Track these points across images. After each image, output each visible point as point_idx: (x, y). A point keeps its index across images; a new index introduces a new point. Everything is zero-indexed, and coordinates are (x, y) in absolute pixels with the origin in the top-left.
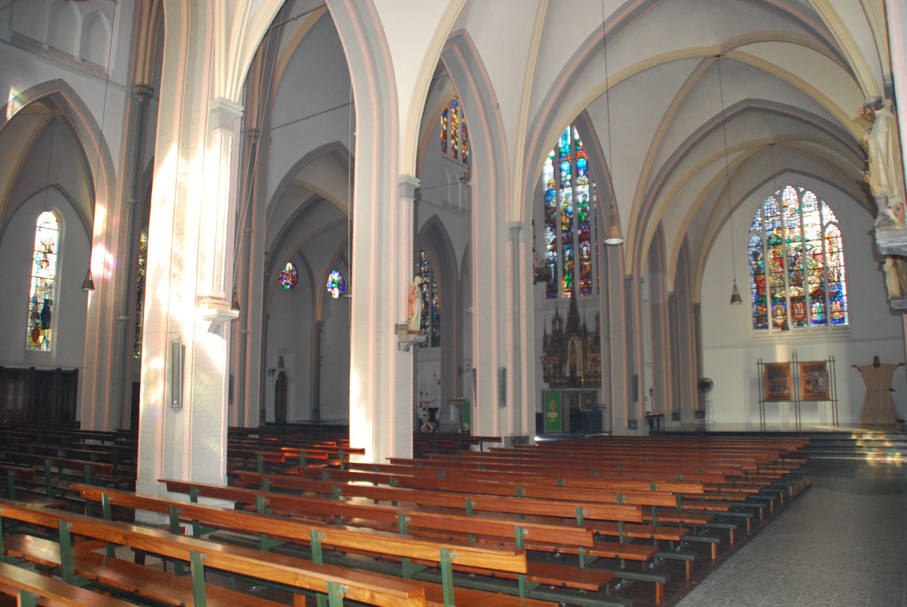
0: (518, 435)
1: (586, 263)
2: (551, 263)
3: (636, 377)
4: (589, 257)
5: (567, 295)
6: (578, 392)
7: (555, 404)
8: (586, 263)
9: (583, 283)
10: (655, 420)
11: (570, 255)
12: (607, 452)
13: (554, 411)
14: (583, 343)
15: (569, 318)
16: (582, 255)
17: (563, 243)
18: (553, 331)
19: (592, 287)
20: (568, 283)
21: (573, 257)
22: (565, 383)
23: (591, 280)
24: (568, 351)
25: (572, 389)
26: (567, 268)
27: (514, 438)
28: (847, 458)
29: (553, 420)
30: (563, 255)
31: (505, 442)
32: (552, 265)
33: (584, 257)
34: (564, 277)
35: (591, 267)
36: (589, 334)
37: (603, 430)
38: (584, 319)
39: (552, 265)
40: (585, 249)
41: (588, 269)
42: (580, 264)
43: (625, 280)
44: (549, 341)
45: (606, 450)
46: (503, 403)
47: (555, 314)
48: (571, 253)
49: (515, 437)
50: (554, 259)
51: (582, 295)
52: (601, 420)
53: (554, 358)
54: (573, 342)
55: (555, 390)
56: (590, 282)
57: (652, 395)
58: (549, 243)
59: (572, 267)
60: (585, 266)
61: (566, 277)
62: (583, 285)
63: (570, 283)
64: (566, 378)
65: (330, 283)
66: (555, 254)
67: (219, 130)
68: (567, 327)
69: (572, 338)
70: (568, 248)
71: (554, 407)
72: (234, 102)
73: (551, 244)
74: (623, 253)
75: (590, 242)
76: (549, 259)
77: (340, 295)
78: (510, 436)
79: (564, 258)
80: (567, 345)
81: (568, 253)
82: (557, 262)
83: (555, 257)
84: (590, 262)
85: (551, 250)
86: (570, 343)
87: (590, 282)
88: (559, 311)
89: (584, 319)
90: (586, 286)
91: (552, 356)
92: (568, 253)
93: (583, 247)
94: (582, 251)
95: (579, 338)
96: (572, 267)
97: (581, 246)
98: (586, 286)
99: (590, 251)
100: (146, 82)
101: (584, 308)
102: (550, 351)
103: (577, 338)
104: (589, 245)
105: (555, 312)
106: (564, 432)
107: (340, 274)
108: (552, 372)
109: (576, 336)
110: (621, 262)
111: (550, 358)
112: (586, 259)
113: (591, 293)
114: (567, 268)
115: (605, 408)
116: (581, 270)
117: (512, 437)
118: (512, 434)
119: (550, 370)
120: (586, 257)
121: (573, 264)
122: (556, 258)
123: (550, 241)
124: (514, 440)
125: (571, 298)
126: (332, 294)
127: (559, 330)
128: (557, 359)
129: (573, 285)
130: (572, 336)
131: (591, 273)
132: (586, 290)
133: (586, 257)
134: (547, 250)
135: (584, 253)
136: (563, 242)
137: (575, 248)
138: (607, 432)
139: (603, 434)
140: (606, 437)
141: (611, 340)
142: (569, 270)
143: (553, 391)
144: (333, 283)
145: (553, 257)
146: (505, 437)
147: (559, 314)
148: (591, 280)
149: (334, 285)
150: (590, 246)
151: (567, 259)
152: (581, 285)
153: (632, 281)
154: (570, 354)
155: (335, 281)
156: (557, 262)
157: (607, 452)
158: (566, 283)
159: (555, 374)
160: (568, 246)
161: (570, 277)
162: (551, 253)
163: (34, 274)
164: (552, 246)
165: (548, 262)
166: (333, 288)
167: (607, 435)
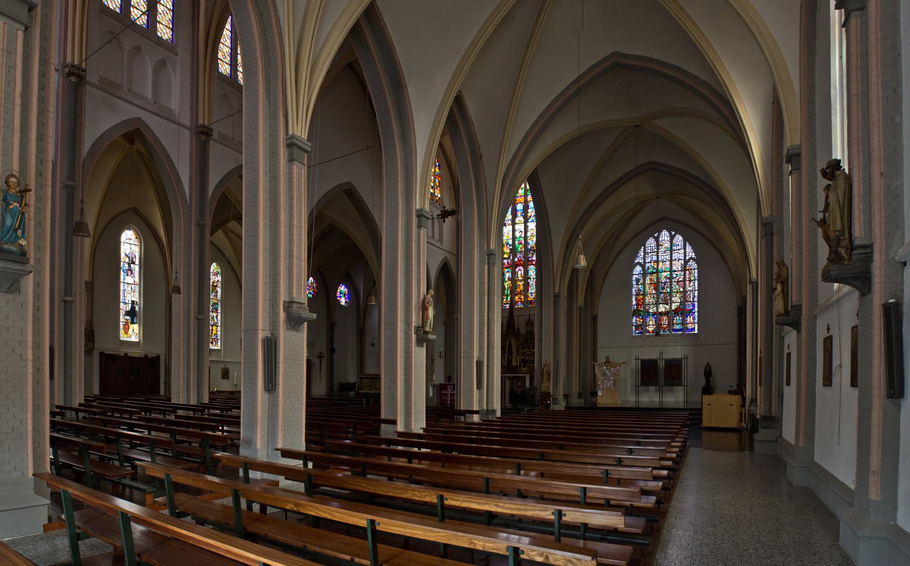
1: (520, 283)
8: (520, 283)
15: (507, 324)
43: (554, 296)
54: (510, 341)
69: (510, 338)
90: (519, 300)
98: (519, 300)
100: (206, 124)
109: (513, 336)
115: (537, 389)
144: (341, 293)
158: (506, 298)
163: (122, 280)
166: (340, 297)
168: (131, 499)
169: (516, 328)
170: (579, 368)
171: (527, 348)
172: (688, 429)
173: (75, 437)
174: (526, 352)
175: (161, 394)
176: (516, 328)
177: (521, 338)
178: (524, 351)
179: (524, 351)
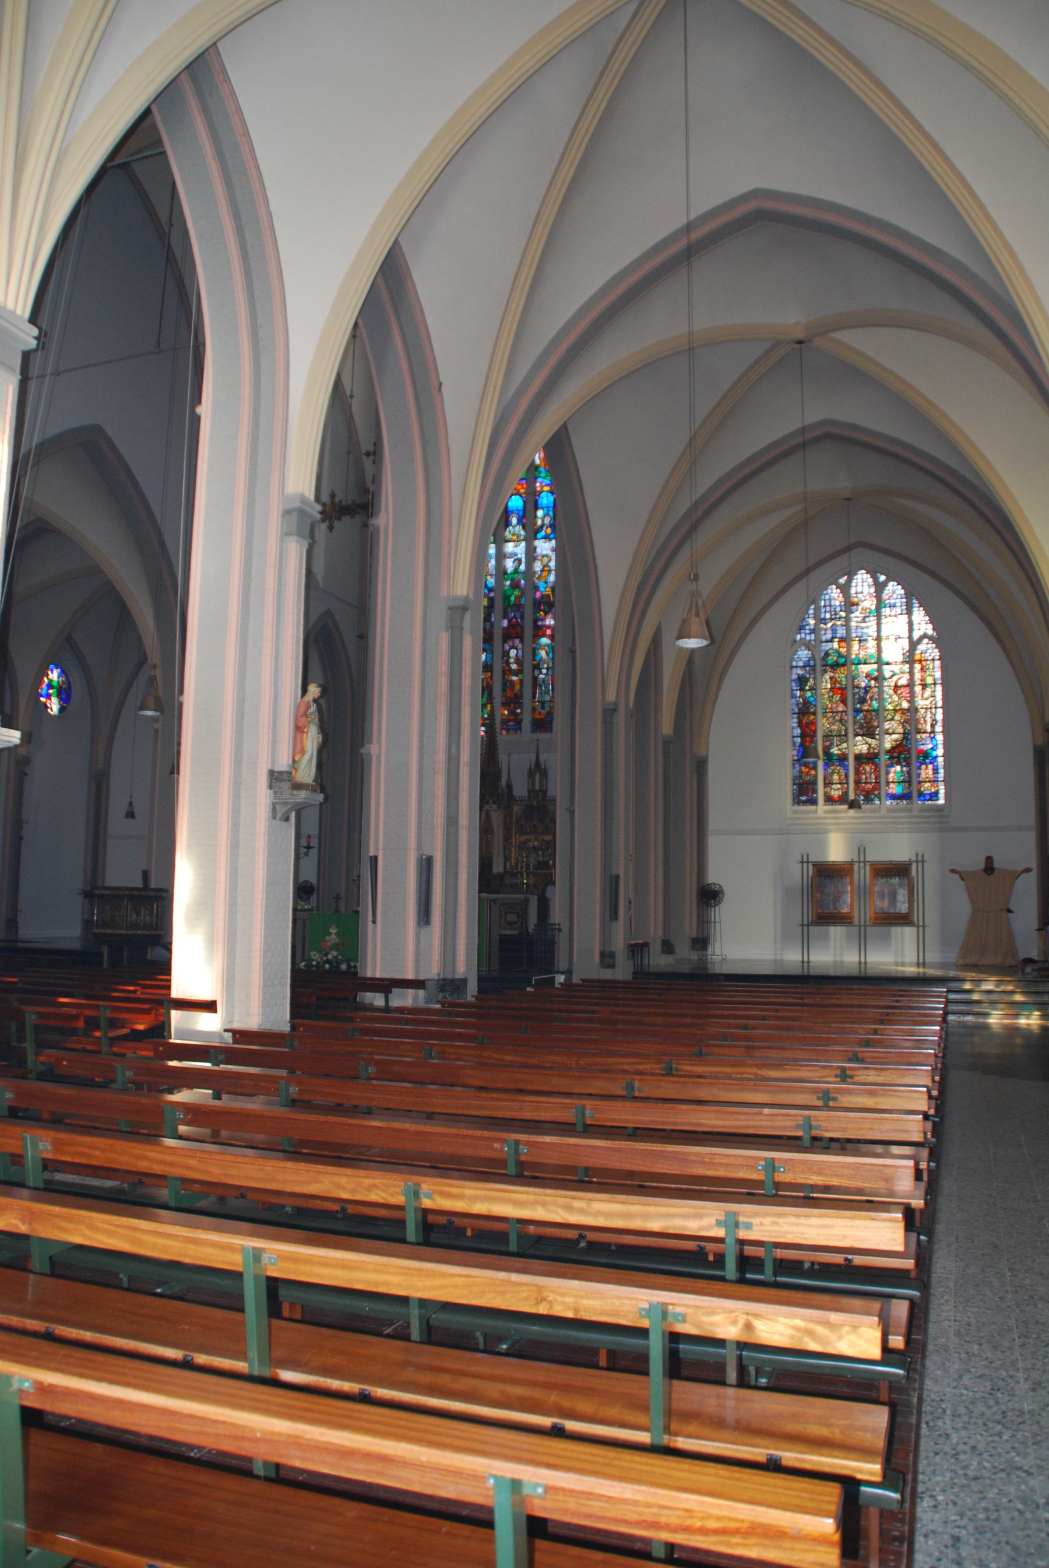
0: (449, 976)
3: (617, 877)
8: (514, 678)
9: (506, 712)
11: (486, 661)
14: (505, 817)
16: (508, 663)
19: (521, 721)
21: (491, 666)
37: (556, 969)
41: (518, 687)
43: (604, 711)
46: (425, 919)
49: (443, 980)
51: (504, 732)
56: (519, 711)
59: (488, 683)
60: (512, 682)
65: (44, 687)
67: (295, 538)
72: (22, 318)
74: (603, 663)
75: (522, 641)
77: (62, 710)
78: (436, 977)
84: (520, 676)
87: (519, 711)
90: (511, 717)
94: (509, 657)
95: (499, 808)
96: (488, 683)
97: (507, 647)
98: (511, 717)
99: (523, 656)
103: (495, 807)
104: (520, 646)
107: (63, 672)
109: (494, 802)
112: (514, 670)
113: (520, 729)
115: (560, 930)
116: (504, 690)
117: (438, 980)
118: (439, 974)
120: (514, 667)
121: (491, 677)
124: (443, 986)
126: (47, 707)
131: (522, 695)
132: (512, 723)
135: (512, 660)
144: (50, 686)
149: (51, 691)
150: (523, 648)
155: (55, 684)
166: (48, 696)
169: (504, 783)
176: (504, 783)
177: (516, 808)
178: (523, 838)
179: (523, 838)
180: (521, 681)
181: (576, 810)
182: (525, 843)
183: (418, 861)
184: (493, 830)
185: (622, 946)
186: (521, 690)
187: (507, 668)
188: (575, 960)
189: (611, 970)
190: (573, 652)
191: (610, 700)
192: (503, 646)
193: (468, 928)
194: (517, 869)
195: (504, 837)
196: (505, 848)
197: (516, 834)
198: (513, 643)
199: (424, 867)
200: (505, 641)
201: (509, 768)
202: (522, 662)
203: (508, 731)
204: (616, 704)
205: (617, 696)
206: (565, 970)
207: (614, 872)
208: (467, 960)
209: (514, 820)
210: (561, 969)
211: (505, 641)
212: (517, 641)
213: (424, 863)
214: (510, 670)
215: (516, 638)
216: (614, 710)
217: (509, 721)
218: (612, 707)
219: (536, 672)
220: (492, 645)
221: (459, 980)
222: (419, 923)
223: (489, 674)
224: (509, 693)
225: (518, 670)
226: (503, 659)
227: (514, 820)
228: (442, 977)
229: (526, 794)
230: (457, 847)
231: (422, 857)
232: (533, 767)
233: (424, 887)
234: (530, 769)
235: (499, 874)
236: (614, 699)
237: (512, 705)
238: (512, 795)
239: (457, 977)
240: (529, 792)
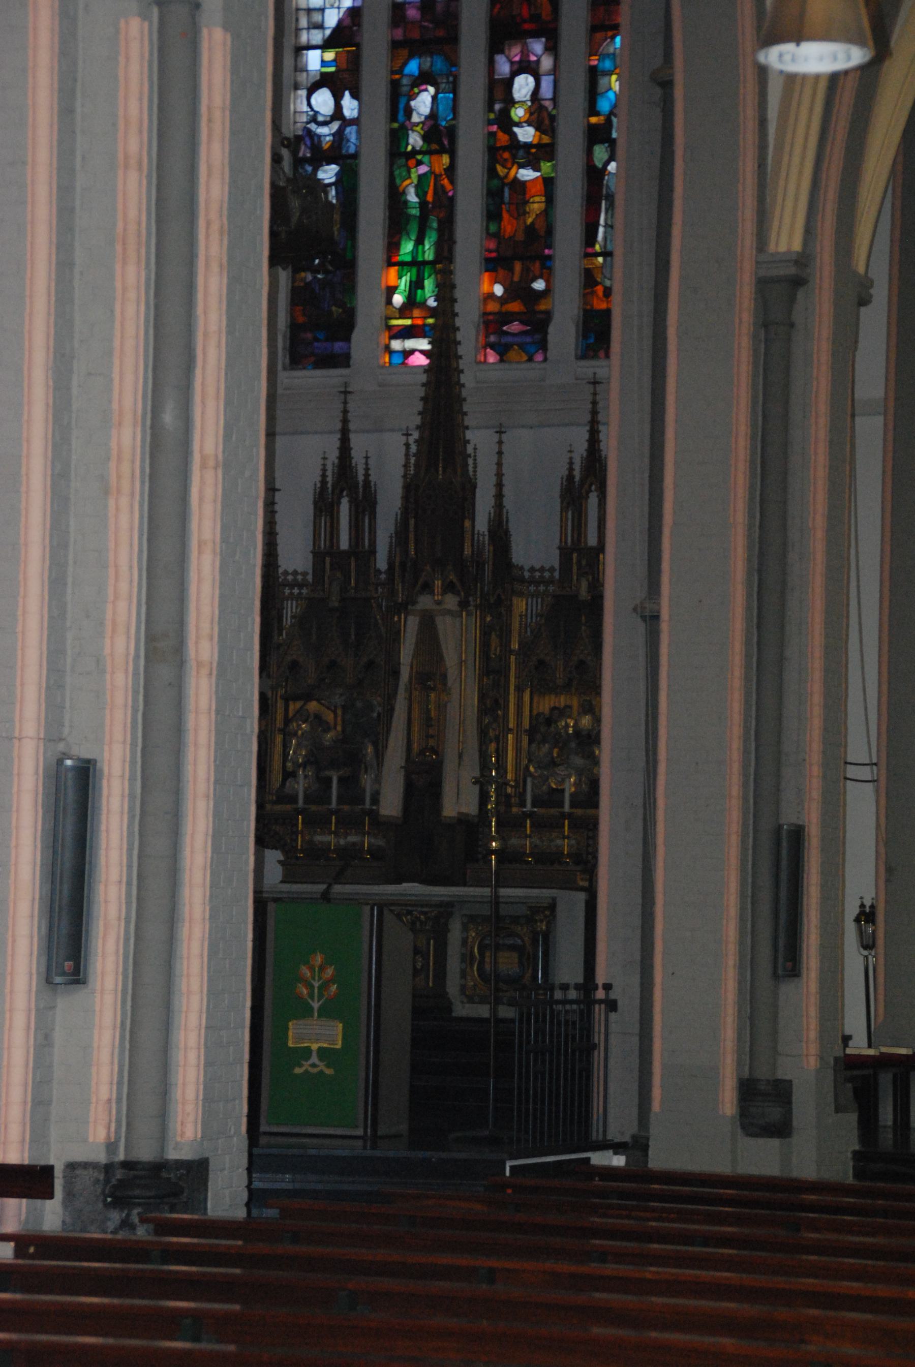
0: (145, 1153)
1: (527, 174)
2: (321, 157)
3: (798, 834)
4: (546, 140)
5: (408, 353)
6: (446, 909)
7: (330, 972)
8: (527, 174)
9: (498, 290)
10: (886, 1080)
11: (433, 116)
12: (611, 1269)
13: (325, 1012)
14: (486, 633)
15: (409, 488)
16: (506, 123)
17: (395, 45)
18: (318, 556)
19: (547, 317)
20: (416, 285)
21: (452, 132)
22: (376, 854)
23: (547, 273)
24: (396, 673)
25: (412, 889)
26: (412, 197)
27: (119, 1174)
28: (371, 1061)
29: (314, 1065)
30: (393, 117)
31: (69, 1195)
32: (328, 173)
33: (514, 136)
34: (393, 246)
35: (550, 200)
36: (522, 580)
37: (596, 1135)
38: (499, 496)
39: (328, 173)
40: (523, 86)
41: (537, 205)
42: (492, 172)
43: (763, 284)
44: (291, 609)
45: (603, 1256)
46: (68, 965)
47: (333, 456)
48: (444, 110)
49: (127, 1165)
50: (339, 135)
51: (492, 358)
52: (587, 1074)
53: (313, 706)
54: (428, 624)
55: (337, 888)
56: (539, 285)
57: (868, 944)
58: (317, 37)
59: (439, 191)
60: (520, 186)
61: (407, 247)
62: (502, 300)
63: (429, 284)
64: (378, 823)
66: (350, 107)
68: (400, 536)
69: (425, 602)
70: (425, 78)
71: (324, 986)
73: (326, 46)
74: (763, 122)
75: (552, 48)
76: (309, 132)
78: (102, 1157)
79: (397, 136)
80: (395, 636)
81: (423, 103)
82: (355, 156)
83: (346, 123)
84: (546, 166)
85: (324, 81)
86: (411, 626)
87: (539, 285)
88: (359, 444)
89: (499, 496)
90: (515, 307)
91: (308, 697)
92: (423, 103)
93: (515, 74)
94: (510, 102)
95: (463, 604)
96: (439, 191)
97: (503, 67)
98: (515, 307)
99: (554, 99)
101: (500, 432)
102: (294, 666)
103: (451, 601)
104: (547, 63)
105: (332, 445)
106: (375, 1140)
108: (300, 785)
109: (449, 588)
110: (748, 167)
111: (293, 707)
112: (527, 146)
113: (543, 345)
114: (412, 197)
115: (612, 1006)
116: (492, 215)
117: (108, 1168)
118: (111, 1147)
119: (288, 775)
120: (526, 134)
121: (451, 170)
122: (351, 132)
123: (320, 26)
124: (122, 1183)
125: (427, 370)
127: (347, 554)
128: (329, 717)
129: (445, 292)
130: (427, 588)
131: (550, 231)
132: (515, 327)
133: (526, 134)
134: (302, 78)
135: (518, 113)
136: (399, 34)
137: (464, 79)
138: (618, 1148)
139: (599, 1159)
140: (609, 1173)
141: (664, 627)
142: (423, 204)
143: (326, 897)
145: (335, 126)
146: (71, 1167)
147: (357, 456)
148: (547, 273)
150: (555, 71)
151: (415, 140)
152: (491, 296)
153: (800, 294)
154: (409, 691)
156: (355, 156)
157: (611, 1269)
158: (404, 284)
159: (319, 795)
160: (427, 62)
161: (429, 253)
162: (323, 101)
164: (330, 55)
165: (304, 152)
167: (619, 1161)
168: (510, 194)
169: (482, 524)
170: (756, 831)
171: (567, 687)
172: (431, 984)
173: (490, 518)
174: (562, 712)
175: (417, 619)
176: (482, 524)
177: (520, 605)
178: (545, 704)
179: (545, 704)
180: (548, 183)
181: (665, 614)
182: (549, 721)
183: (46, 776)
184: (444, 677)
185: (813, 1062)
186: (548, 212)
187: (503, 138)
188: (656, 1106)
189: (775, 1143)
190: (667, 85)
191: (783, 248)
192: (491, 63)
193: (214, 993)
194: (523, 804)
195: (482, 697)
196: (483, 733)
197: (519, 690)
198: (525, 52)
199: (71, 795)
200: (495, 47)
201: (499, 475)
202: (553, 118)
203: (502, 351)
204: (803, 260)
205: (809, 231)
206: (627, 1138)
207: (789, 818)
208: (209, 1099)
209: (515, 646)
210: (614, 1134)
211: (495, 47)
212: (537, 46)
213: (70, 780)
214: (515, 144)
215: (536, 35)
216: (798, 282)
217: (506, 318)
218: (792, 270)
219: (600, 153)
220: (453, 61)
221: (180, 1164)
222: (49, 981)
223: (446, 159)
224: (508, 226)
225: (539, 146)
226: (491, 109)
227: (515, 646)
228: (121, 1156)
229: (553, 559)
230: (179, 729)
231: (60, 762)
232: (577, 473)
233: (68, 856)
234: (570, 477)
235: (463, 820)
236: (797, 246)
237: (518, 267)
238: (509, 565)
239: (173, 1155)
240: (565, 553)
